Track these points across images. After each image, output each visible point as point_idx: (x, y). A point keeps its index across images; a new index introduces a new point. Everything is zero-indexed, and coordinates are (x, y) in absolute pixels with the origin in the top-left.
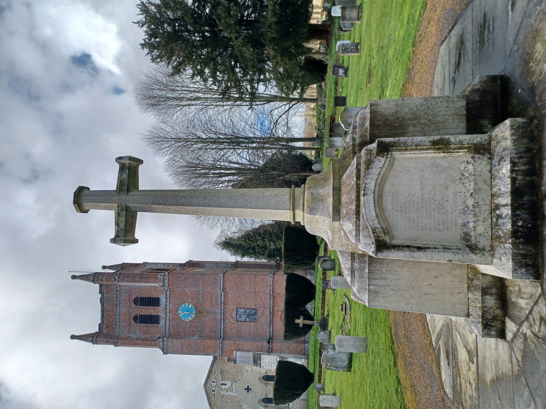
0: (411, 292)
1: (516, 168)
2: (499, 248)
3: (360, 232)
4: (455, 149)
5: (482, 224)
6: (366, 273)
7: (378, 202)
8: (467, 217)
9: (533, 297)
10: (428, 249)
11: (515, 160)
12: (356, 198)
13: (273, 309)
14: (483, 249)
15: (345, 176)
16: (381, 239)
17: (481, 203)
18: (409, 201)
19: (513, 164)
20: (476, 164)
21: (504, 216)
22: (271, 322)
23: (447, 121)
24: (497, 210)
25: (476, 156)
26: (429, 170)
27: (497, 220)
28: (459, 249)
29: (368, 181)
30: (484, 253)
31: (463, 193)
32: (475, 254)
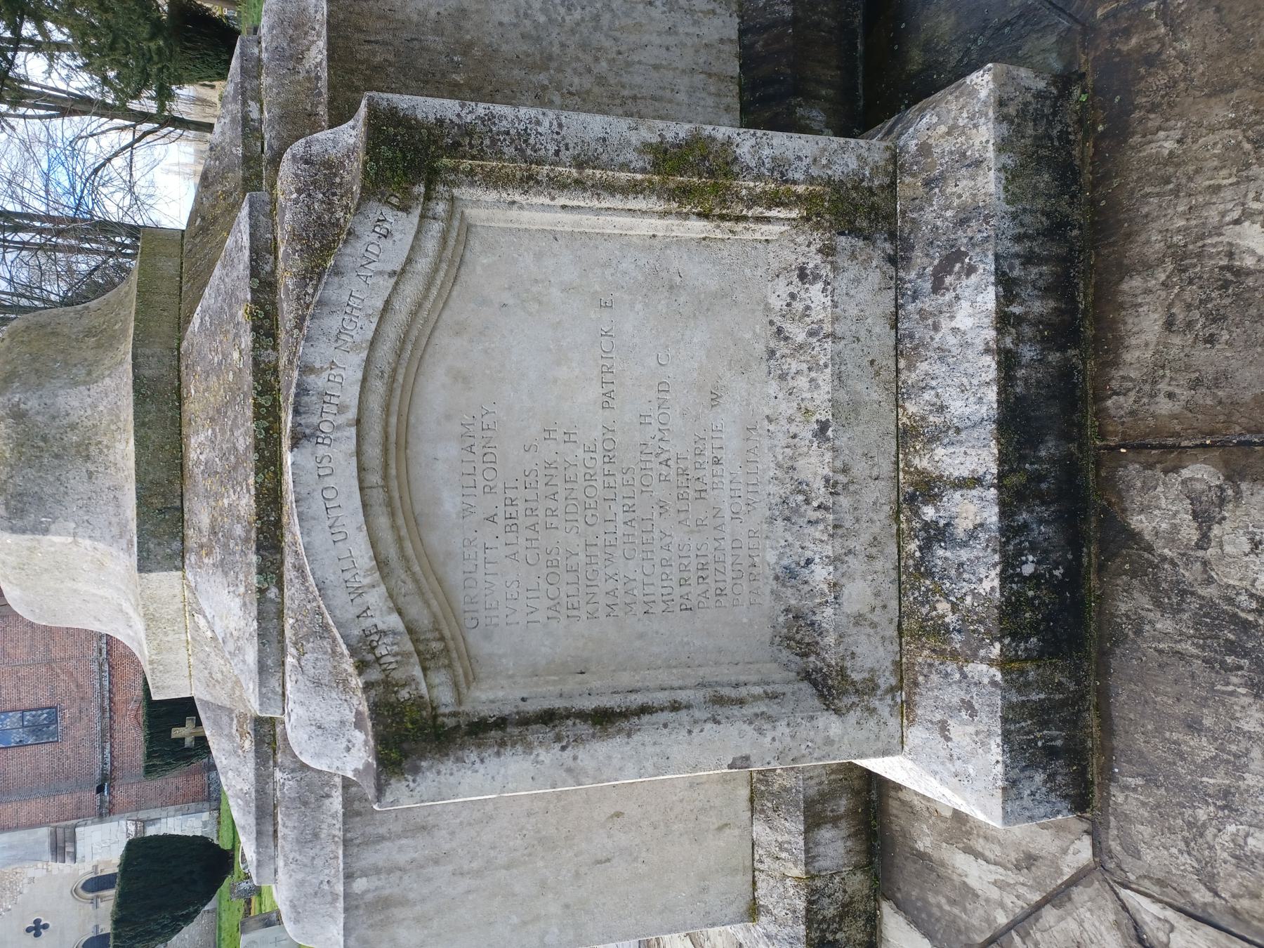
0: (541, 864)
1: (1016, 309)
2: (935, 677)
3: (283, 651)
4: (753, 201)
5: (864, 567)
6: (334, 816)
7: (385, 477)
8: (799, 537)
9: (1041, 870)
10: (646, 718)
11: (1012, 268)
12: (257, 449)
13: (111, 700)
14: (870, 687)
15: (196, 320)
16: (404, 694)
17: (860, 469)
18: (548, 466)
19: (1007, 286)
20: (842, 283)
21: (960, 533)
22: (108, 733)
23: (668, 94)
24: (925, 503)
25: (843, 241)
26: (639, 306)
27: (926, 547)
28: (773, 697)
29: (319, 353)
30: (875, 703)
31: (783, 422)
32: (837, 711)
